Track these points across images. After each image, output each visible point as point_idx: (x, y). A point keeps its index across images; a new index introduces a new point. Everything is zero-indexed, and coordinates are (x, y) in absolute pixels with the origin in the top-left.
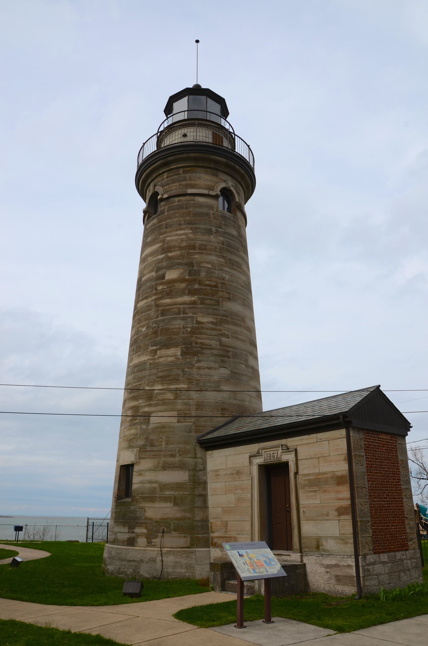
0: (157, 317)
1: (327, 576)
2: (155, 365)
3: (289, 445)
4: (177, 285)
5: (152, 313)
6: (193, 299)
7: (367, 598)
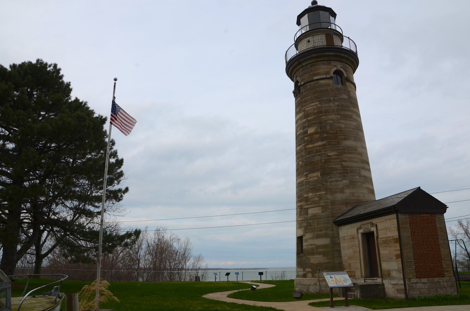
0: (306, 155)
1: (393, 290)
2: (308, 183)
3: (374, 222)
4: (314, 136)
5: (303, 153)
6: (324, 143)
7: (410, 299)
